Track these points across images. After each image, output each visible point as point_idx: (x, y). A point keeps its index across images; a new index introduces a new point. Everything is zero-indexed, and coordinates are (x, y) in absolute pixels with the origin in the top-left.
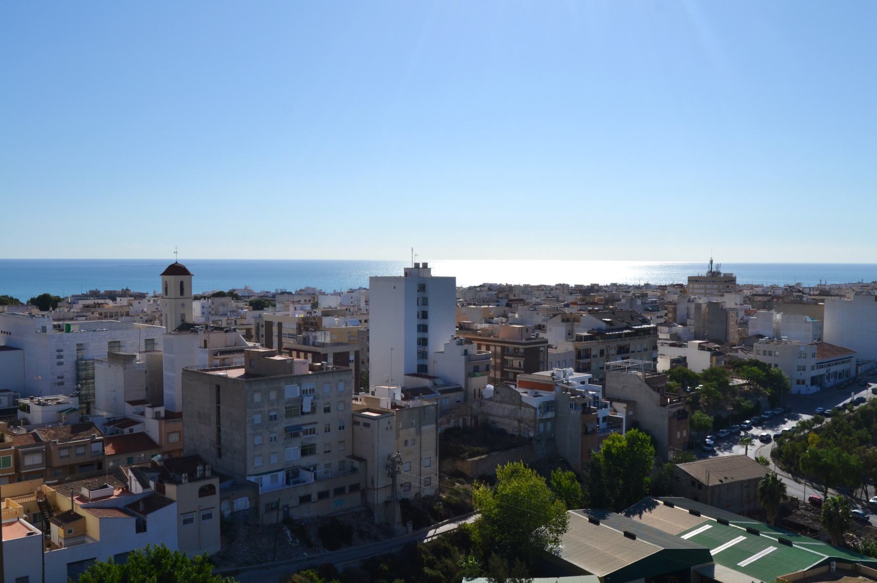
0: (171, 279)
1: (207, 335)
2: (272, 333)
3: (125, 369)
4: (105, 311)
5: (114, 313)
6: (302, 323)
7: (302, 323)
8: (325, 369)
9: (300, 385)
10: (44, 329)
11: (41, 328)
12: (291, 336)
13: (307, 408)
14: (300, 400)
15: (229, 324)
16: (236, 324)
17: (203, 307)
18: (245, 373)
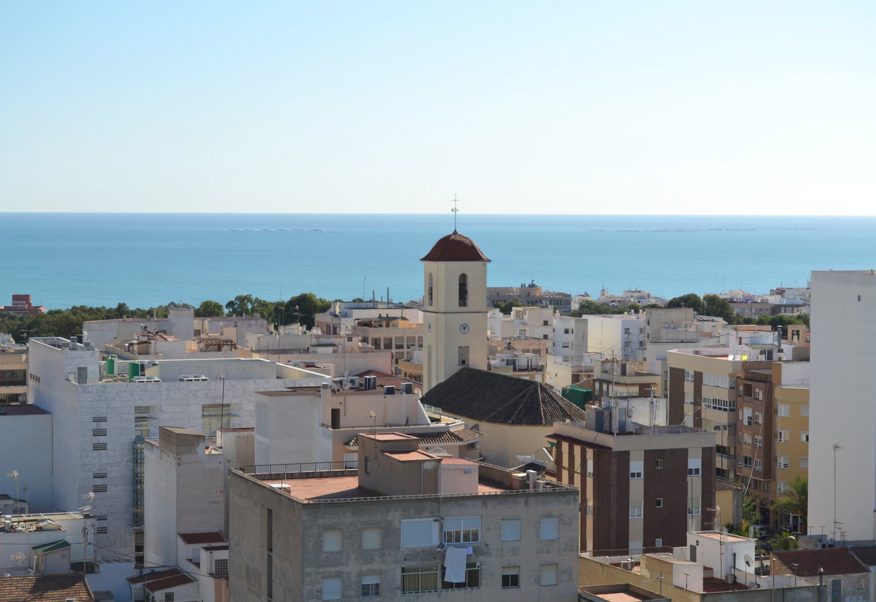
0: (440, 267)
1: (341, 399)
2: (683, 395)
3: (179, 464)
4: (399, 335)
5: (405, 339)
6: (741, 374)
7: (741, 374)
8: (531, 486)
9: (440, 520)
10: (82, 375)
11: (76, 370)
12: (718, 405)
13: (456, 573)
14: (438, 555)
15: (606, 372)
16: (624, 373)
17: (627, 331)
18: (359, 486)
